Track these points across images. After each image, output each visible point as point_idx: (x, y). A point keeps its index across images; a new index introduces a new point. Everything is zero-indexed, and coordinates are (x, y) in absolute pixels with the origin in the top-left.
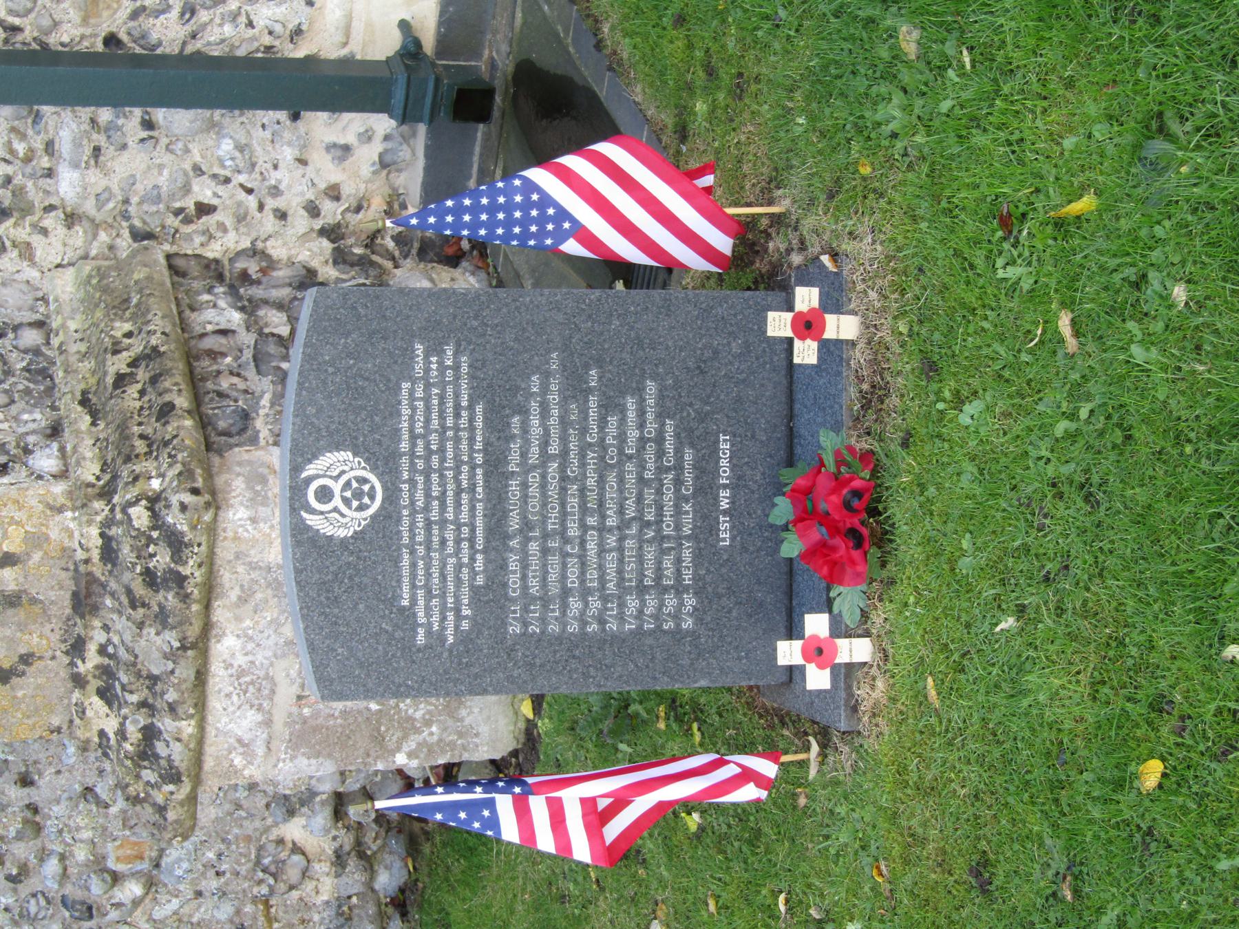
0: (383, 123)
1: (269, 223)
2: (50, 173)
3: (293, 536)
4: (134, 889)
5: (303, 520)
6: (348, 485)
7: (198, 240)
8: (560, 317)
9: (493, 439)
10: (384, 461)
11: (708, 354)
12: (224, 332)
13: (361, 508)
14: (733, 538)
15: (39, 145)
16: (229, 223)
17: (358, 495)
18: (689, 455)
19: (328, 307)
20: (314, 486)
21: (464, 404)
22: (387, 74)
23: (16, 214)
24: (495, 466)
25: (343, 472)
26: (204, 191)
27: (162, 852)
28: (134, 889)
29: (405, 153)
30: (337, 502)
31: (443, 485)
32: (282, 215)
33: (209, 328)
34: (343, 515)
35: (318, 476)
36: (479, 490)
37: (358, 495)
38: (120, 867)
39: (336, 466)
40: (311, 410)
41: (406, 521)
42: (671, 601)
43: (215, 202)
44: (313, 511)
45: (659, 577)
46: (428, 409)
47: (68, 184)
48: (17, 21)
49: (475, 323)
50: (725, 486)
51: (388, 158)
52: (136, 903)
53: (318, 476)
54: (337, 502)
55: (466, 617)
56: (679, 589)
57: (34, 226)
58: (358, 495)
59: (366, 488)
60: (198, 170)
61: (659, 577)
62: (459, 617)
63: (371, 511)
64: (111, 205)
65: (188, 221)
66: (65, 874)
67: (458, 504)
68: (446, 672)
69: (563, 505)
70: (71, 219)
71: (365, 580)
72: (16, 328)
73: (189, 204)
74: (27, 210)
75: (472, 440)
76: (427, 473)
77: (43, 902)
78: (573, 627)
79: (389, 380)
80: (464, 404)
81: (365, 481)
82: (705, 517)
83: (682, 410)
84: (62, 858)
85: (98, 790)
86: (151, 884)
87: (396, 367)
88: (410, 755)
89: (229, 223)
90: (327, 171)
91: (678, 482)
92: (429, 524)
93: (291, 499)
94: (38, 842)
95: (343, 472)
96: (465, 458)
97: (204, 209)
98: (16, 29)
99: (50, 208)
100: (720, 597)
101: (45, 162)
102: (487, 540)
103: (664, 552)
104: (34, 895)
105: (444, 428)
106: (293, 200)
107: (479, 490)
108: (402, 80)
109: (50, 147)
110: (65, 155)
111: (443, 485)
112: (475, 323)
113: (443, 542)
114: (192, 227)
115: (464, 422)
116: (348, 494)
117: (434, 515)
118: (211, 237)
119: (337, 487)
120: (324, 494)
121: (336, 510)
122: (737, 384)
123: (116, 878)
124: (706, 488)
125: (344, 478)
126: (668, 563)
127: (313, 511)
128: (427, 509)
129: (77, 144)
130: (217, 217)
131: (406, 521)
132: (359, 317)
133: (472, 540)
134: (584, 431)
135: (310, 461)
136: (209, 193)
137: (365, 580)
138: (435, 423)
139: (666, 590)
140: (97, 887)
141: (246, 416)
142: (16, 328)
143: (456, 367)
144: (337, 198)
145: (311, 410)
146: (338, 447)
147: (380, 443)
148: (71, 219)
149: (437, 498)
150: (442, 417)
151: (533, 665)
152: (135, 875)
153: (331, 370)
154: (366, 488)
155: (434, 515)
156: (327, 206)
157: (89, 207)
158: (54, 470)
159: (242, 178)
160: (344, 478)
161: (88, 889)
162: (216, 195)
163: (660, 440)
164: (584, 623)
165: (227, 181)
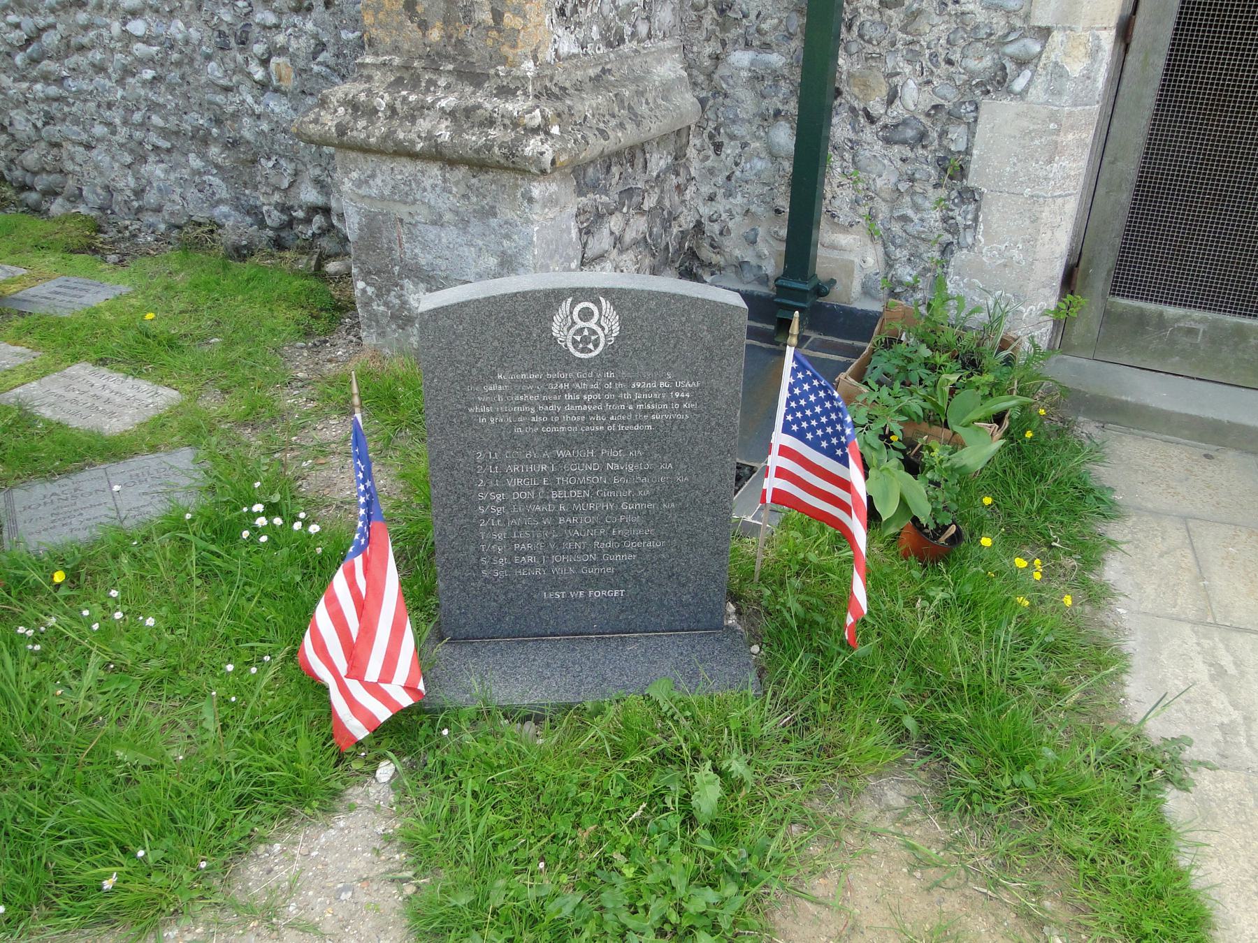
0: (772, 267)
1: (706, 190)
2: (748, 45)
3: (553, 291)
4: (259, 74)
5: (565, 299)
6: (594, 333)
7: (698, 142)
8: (714, 481)
9: (626, 437)
10: (611, 359)
11: (683, 580)
12: (645, 166)
13: (574, 342)
14: (549, 600)
15: (768, 39)
16: (708, 163)
17: (585, 340)
18: (610, 570)
19: (731, 316)
20: (591, 305)
21: (653, 417)
22: (809, 274)
23: (720, 20)
24: (605, 439)
25: (603, 329)
26: (730, 150)
27: (285, 94)
28: (259, 74)
29: (749, 276)
30: (580, 324)
31: (592, 403)
32: (711, 198)
33: (648, 156)
34: (569, 330)
35: (600, 310)
36: (588, 428)
37: (585, 340)
38: (272, 65)
39: (606, 323)
40: (653, 304)
41: (564, 376)
42: (500, 536)
43: (723, 156)
44: (572, 306)
45: (521, 554)
46: (650, 391)
47: (741, 58)
48: (855, 29)
49: (713, 424)
50: (586, 594)
51: (745, 266)
52: (249, 75)
53: (600, 310)
54: (580, 324)
55: (488, 421)
56: (511, 566)
57: (714, 32)
58: (585, 341)
59: (591, 346)
60: (744, 145)
61: (521, 554)
62: (488, 415)
63: (572, 350)
64: (724, 86)
65: (711, 137)
66: (265, 27)
67: (578, 414)
68: (445, 407)
69: (576, 487)
70: (716, 58)
71: (518, 346)
72: (648, 18)
73: (722, 138)
74: (724, 28)
75: (626, 423)
76: (602, 390)
77: (245, 11)
78: (482, 497)
79: (674, 362)
80: (653, 417)
81: (596, 346)
82: (564, 583)
83: (643, 565)
84: (277, 26)
85: (325, 53)
86: (264, 86)
87: (683, 367)
88: (364, 291)
89: (708, 163)
90: (738, 226)
91: (590, 564)
92: (561, 392)
93: (583, 289)
94: (286, 10)
95: (603, 329)
96: (612, 418)
97: (718, 147)
98: (849, 28)
99: (724, 44)
100: (505, 594)
101: (756, 43)
102: (548, 434)
103: (539, 557)
104: (250, 5)
105: (634, 403)
106: (721, 205)
107: (588, 428)
108: (807, 287)
109: (766, 47)
110: (760, 56)
111: (592, 403)
112: (713, 424)
113: (548, 403)
114: (707, 140)
115: (639, 416)
116: (586, 333)
117: (569, 397)
118: (699, 151)
119: (592, 324)
120: (586, 315)
121: (574, 323)
122: (661, 600)
123: (265, 63)
124: (587, 582)
125: (599, 330)
126: (531, 559)
127: (572, 306)
128: (573, 391)
129: (767, 65)
130: (713, 156)
131: (564, 376)
132: (723, 340)
133: (549, 423)
134: (630, 500)
135: (612, 304)
136: (729, 151)
137: (518, 346)
138: (638, 396)
139: (511, 558)
140: (258, 49)
141: (595, 187)
142: (648, 18)
143: (681, 411)
144: (721, 233)
145: (653, 304)
146: (623, 323)
147: (625, 356)
148: (716, 58)
149: (582, 398)
150: (644, 401)
151: (452, 468)
152: (268, 75)
153: (684, 319)
154: (591, 346)
155: (569, 397)
156: (716, 227)
157: (723, 70)
158: (561, 51)
159: (738, 173)
160: (599, 330)
161: (257, 42)
162: (728, 155)
163: (622, 550)
164: (484, 504)
165: (737, 164)
